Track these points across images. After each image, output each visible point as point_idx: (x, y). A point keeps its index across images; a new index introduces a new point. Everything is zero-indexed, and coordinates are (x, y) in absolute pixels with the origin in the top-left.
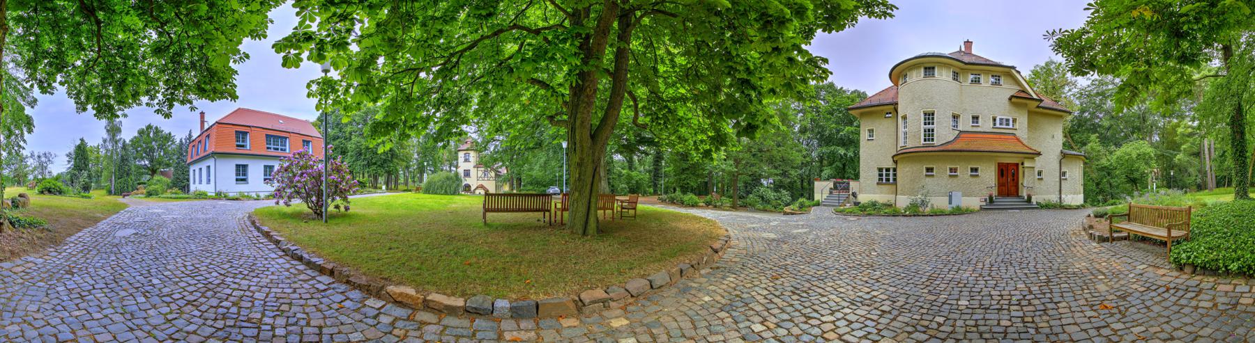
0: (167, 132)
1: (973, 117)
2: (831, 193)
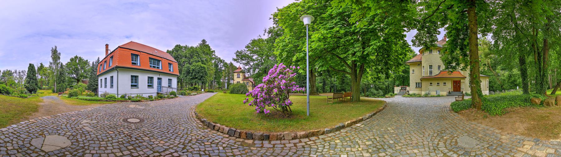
0: (86, 60)
2: (400, 91)
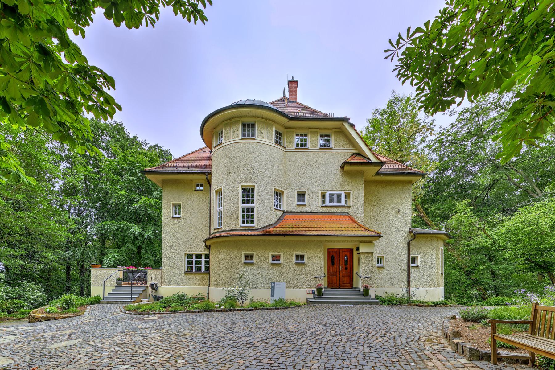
2: (119, 285)
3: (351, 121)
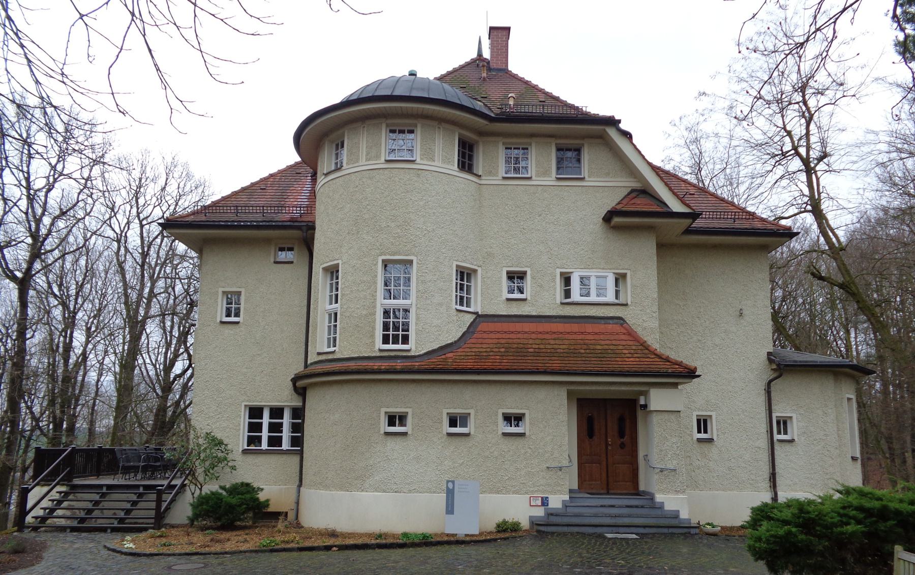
1: (511, 276)
3: (622, 126)
